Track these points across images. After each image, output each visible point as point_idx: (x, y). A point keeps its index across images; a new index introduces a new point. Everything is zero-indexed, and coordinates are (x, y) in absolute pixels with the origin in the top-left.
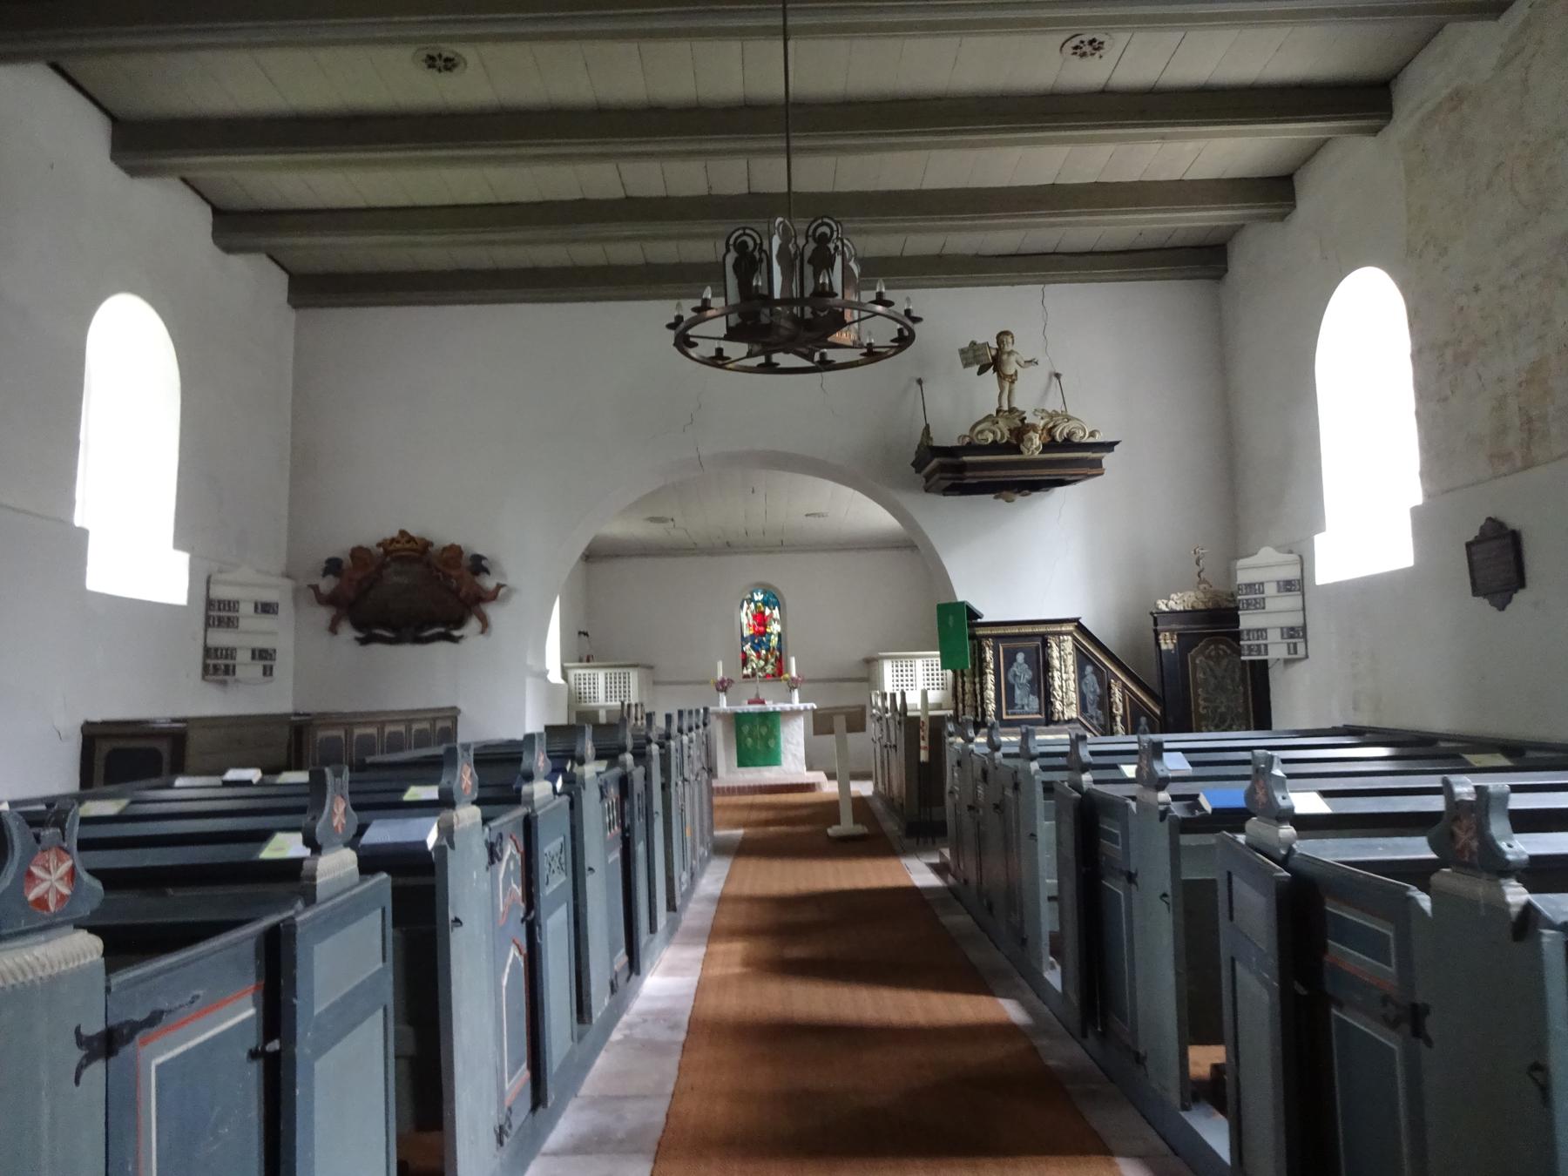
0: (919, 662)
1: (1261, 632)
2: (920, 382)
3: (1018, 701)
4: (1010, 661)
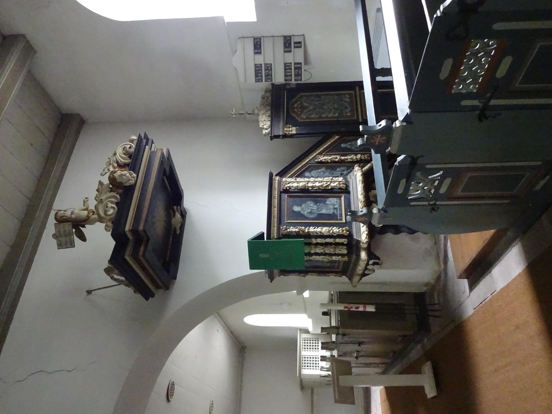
0: (303, 353)
1: (287, 67)
2: (89, 292)
3: (331, 212)
4: (299, 215)
